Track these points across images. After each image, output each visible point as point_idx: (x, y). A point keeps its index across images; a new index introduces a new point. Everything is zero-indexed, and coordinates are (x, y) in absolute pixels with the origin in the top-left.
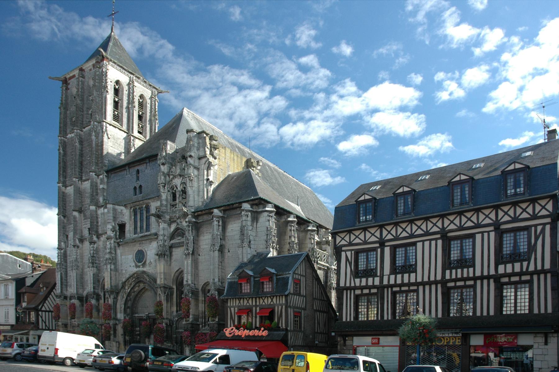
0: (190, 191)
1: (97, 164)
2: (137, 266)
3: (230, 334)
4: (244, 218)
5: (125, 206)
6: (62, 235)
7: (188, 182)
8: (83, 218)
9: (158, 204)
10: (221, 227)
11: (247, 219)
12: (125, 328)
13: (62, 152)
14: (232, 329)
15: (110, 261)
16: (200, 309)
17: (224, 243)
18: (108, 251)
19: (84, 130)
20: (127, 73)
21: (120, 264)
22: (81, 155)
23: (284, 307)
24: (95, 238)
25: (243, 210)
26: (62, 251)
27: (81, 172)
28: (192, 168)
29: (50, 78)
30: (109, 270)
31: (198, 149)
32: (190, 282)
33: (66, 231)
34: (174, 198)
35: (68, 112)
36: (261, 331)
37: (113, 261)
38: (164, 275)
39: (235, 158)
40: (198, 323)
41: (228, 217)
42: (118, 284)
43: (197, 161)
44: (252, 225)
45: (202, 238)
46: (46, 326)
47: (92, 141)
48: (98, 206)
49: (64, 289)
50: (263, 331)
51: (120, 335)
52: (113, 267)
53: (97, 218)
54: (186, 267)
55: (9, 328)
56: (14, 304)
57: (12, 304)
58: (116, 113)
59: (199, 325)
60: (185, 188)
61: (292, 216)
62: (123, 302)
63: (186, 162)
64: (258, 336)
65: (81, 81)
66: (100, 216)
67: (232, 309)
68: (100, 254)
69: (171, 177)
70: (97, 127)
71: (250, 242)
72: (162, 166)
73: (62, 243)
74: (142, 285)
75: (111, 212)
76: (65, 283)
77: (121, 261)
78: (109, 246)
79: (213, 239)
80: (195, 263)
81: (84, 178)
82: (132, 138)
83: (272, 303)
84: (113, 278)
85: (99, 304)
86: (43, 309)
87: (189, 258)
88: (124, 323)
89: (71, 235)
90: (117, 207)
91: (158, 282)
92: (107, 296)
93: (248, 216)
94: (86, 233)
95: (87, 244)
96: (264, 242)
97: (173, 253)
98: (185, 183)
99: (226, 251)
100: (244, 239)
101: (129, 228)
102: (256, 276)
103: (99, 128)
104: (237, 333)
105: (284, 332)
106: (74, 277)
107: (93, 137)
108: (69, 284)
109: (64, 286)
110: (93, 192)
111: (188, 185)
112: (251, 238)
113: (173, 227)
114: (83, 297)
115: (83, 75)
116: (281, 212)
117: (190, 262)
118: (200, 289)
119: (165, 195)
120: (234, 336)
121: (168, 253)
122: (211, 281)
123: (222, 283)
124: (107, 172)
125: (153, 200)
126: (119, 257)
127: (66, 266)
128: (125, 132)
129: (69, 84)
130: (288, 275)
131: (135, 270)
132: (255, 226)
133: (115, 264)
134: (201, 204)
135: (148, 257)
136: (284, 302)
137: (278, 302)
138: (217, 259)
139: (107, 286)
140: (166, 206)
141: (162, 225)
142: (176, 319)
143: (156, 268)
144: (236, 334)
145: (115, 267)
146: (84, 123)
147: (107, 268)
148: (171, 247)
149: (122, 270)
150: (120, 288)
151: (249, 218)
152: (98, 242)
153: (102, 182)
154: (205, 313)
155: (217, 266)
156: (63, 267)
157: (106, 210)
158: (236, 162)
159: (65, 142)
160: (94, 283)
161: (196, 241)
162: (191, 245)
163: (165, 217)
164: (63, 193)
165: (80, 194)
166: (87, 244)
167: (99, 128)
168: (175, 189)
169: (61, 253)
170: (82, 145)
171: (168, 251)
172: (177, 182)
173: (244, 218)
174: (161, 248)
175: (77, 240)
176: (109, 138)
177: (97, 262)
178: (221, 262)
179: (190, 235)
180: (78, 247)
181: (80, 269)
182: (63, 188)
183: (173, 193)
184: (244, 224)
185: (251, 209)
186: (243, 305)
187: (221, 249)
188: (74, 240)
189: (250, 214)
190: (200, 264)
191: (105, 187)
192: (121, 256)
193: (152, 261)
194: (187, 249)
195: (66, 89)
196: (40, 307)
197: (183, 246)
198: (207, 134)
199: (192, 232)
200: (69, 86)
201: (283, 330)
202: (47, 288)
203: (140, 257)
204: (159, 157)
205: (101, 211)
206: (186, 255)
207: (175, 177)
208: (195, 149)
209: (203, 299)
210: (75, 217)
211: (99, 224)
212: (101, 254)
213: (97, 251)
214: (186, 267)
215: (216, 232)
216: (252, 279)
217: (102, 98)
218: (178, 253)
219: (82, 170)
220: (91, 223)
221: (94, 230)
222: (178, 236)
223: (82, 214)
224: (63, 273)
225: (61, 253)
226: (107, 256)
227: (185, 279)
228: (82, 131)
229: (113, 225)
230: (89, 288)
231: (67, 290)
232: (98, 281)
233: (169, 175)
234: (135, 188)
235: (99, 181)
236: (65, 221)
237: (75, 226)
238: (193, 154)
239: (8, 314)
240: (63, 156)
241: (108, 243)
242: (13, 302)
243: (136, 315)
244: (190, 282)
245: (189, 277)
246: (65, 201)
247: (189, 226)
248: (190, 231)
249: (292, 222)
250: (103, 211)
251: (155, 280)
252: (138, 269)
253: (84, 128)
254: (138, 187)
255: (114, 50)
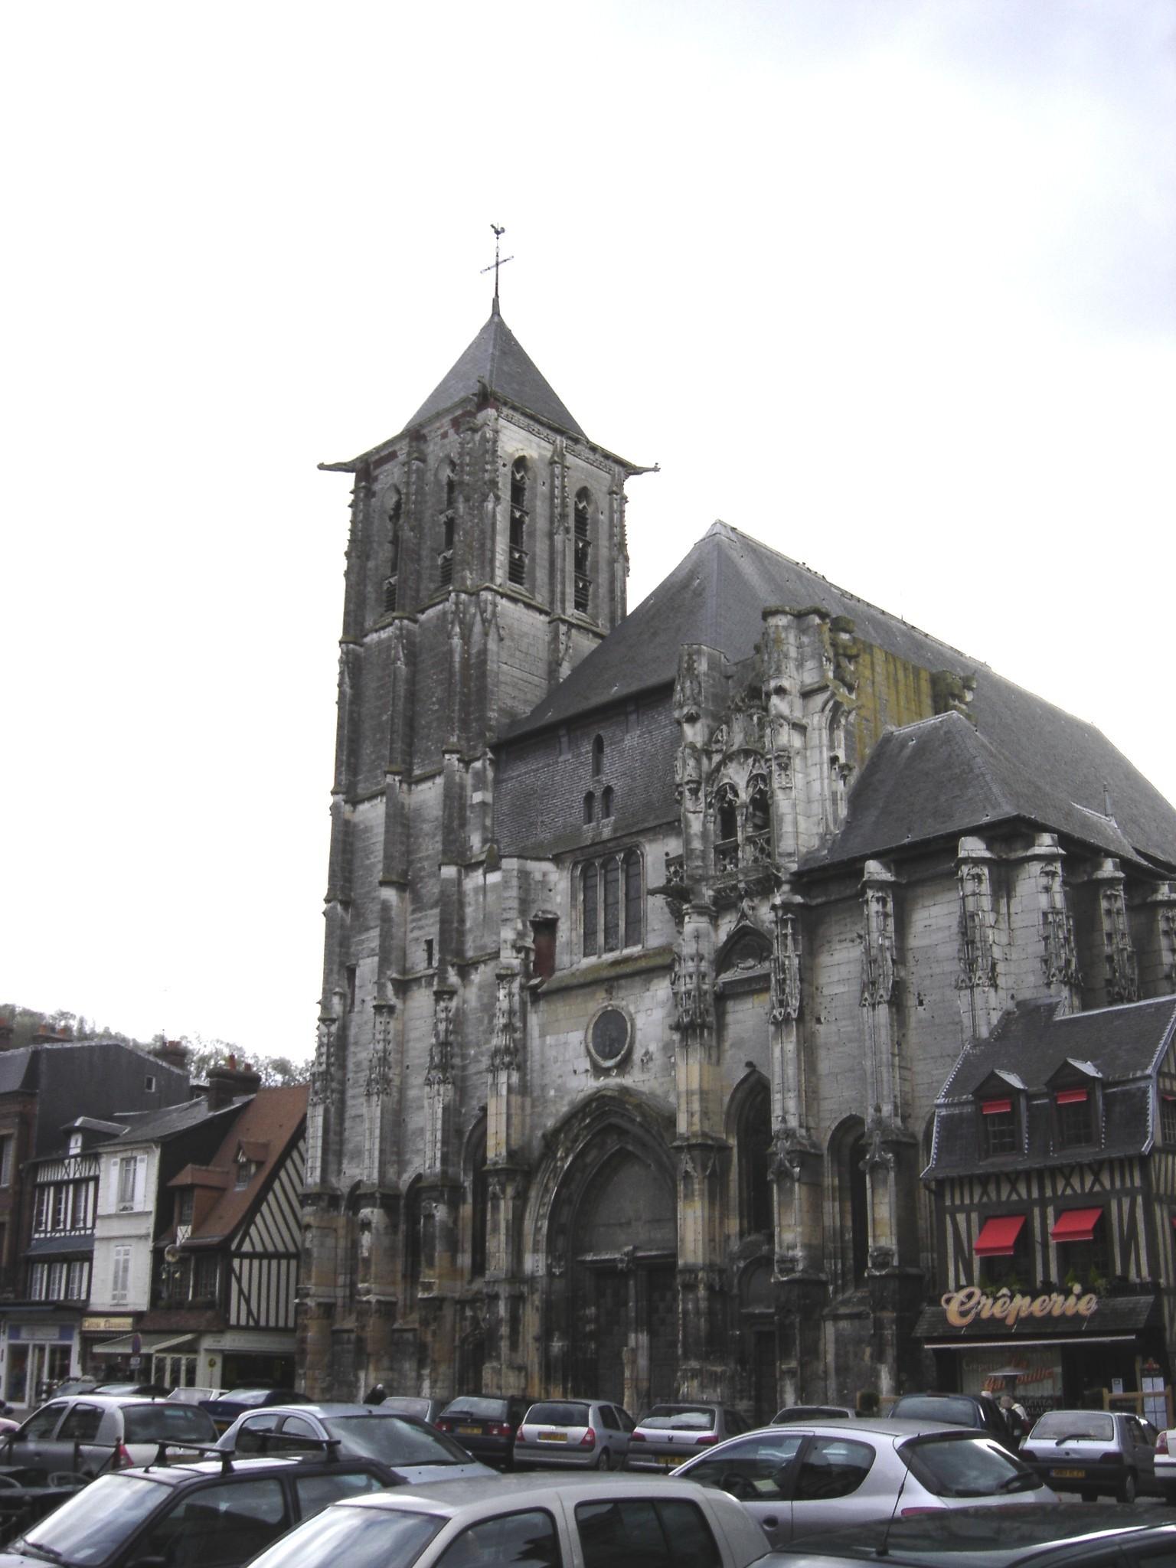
0: (783, 803)
1: (465, 725)
2: (598, 1071)
3: (963, 1314)
4: (970, 886)
5: (557, 860)
6: (335, 968)
7: (775, 775)
8: (410, 908)
9: (673, 846)
10: (891, 921)
11: (979, 891)
12: (548, 1309)
13: (348, 690)
14: (970, 1296)
15: (507, 1059)
16: (828, 1221)
17: (903, 974)
18: (502, 1021)
19: (422, 617)
20: (545, 432)
21: (537, 1066)
22: (412, 697)
23: (1140, 1199)
24: (453, 978)
25: (965, 861)
26: (334, 1028)
27: (409, 753)
28: (786, 727)
29: (322, 467)
30: (504, 1092)
31: (800, 666)
32: (793, 1122)
33: (347, 954)
34: (728, 826)
35: (371, 564)
36: (1072, 1300)
37: (515, 1056)
38: (702, 1100)
39: (901, 674)
40: (823, 1277)
41: (912, 885)
42: (530, 1142)
43: (798, 702)
44: (995, 909)
45: (824, 959)
46: (249, 1312)
47: (451, 652)
48: (469, 867)
49: (333, 1167)
50: (1079, 1297)
51: (529, 1339)
52: (515, 1078)
53: (461, 904)
54: (777, 1068)
55: (126, 1323)
56: (151, 1231)
57: (143, 1231)
58: (517, 556)
59: (824, 1284)
60: (761, 791)
61: (1046, 839)
62: (545, 1210)
63: (766, 709)
64: (1063, 1315)
65: (418, 470)
66: (470, 898)
67: (961, 1218)
68: (469, 1030)
69: (717, 758)
70: (466, 606)
71: (994, 966)
72: (687, 727)
73: (336, 1000)
74: (613, 1145)
75: (515, 882)
76: (335, 1149)
77: (542, 1052)
78: (504, 1004)
79: (872, 961)
80: (808, 1049)
81: (417, 772)
82: (563, 628)
83: (1097, 1188)
84: (515, 1120)
85: (455, 1222)
86: (247, 1247)
87: (789, 1035)
88: (548, 1293)
89: (367, 967)
90: (532, 865)
91: (682, 1127)
92: (494, 1187)
93: (980, 881)
94: (418, 959)
95: (422, 999)
96: (1038, 965)
97: (730, 1018)
98: (765, 779)
99: (912, 1001)
100: (975, 960)
101: (567, 933)
102: (1033, 1089)
103: (472, 610)
104: (989, 1308)
105: (1150, 1298)
106: (372, 1120)
107: (456, 641)
108: (349, 1147)
109: (331, 1158)
110: (450, 816)
111: (775, 785)
112: (997, 952)
113: (728, 925)
114: (397, 1197)
115: (421, 452)
116: (1079, 854)
117: (791, 1046)
118: (826, 1145)
119: (698, 820)
120: (978, 1321)
121: (711, 1019)
122: (869, 1115)
123: (904, 1119)
124: (496, 748)
125: (650, 836)
126: (535, 1043)
127: (343, 1082)
128: (541, 611)
129: (376, 479)
130: (1142, 1084)
131: (589, 1084)
132: (1004, 910)
133: (521, 1068)
134: (815, 842)
135: (639, 1036)
136: (1137, 1182)
137: (1118, 1184)
138: (884, 1036)
139: (496, 1149)
140: (704, 856)
141: (693, 924)
142: (742, 1264)
143: (677, 1081)
144: (985, 1315)
145: (523, 1079)
146: (423, 594)
147: (495, 1085)
148: (724, 997)
149: (544, 1088)
150: (536, 1154)
151: (986, 887)
152: (461, 991)
153: (480, 783)
154: (842, 1234)
155: (885, 1057)
156: (334, 1085)
157: (494, 878)
158: (901, 687)
159: (357, 657)
160: (444, 1142)
161: (807, 973)
162: (793, 987)
163: (701, 896)
164: (347, 823)
165: (404, 825)
166: (422, 999)
167: (472, 610)
168: (730, 796)
169: (329, 1035)
170: (415, 664)
171: (712, 1010)
172: (738, 775)
173: (970, 886)
174: (690, 1004)
175: (390, 987)
176: (501, 639)
177: (457, 1061)
178: (899, 1044)
179: (790, 956)
180: (391, 1009)
181: (395, 1094)
182: (348, 808)
183: (722, 810)
184: (971, 907)
185: (987, 855)
186: (999, 1202)
187: (897, 1001)
188: (381, 987)
189: (986, 871)
190: (822, 1053)
191: (489, 797)
192: (543, 1035)
193: (652, 1048)
194: (782, 1004)
195: (366, 496)
196: (233, 1247)
197: (767, 989)
198: (823, 616)
199: (795, 940)
200: (377, 487)
201: (1143, 1288)
202: (260, 1164)
203: (612, 1040)
204: (678, 696)
205: (475, 879)
206: (777, 1023)
207: (728, 758)
208: (792, 665)
209: (836, 1182)
210: (385, 907)
211: (468, 925)
212: (472, 1032)
213: (457, 1021)
214: (777, 1068)
215: (876, 939)
216: (1023, 1102)
217: (481, 519)
218: (747, 1017)
219: (410, 745)
220: (444, 922)
221: (454, 952)
222: (744, 957)
223: (407, 895)
224: (333, 1109)
225: (329, 1035)
226: (499, 1041)
227: (777, 1110)
228: (415, 621)
229: (520, 926)
230: (426, 1158)
231: (339, 1172)
232: (464, 1135)
233: (709, 754)
234: (590, 797)
235: (469, 780)
236: (348, 920)
237: (385, 936)
238: (786, 683)
239: (126, 1269)
240: (352, 703)
241: (502, 994)
242: (148, 1226)
243: (589, 1258)
244: (793, 1122)
245: (792, 1105)
246: (352, 852)
247: (782, 922)
248: (789, 941)
249: (1111, 882)
250: (480, 880)
251: (671, 1121)
252: (602, 1081)
253: (422, 612)
254: (598, 794)
255: (505, 368)
